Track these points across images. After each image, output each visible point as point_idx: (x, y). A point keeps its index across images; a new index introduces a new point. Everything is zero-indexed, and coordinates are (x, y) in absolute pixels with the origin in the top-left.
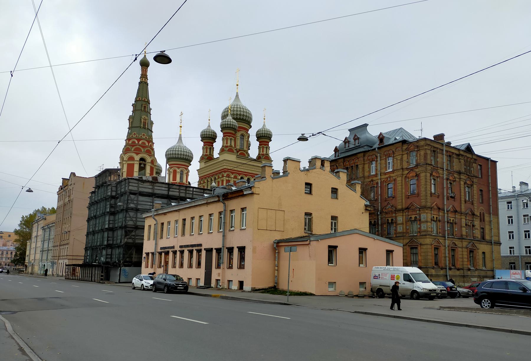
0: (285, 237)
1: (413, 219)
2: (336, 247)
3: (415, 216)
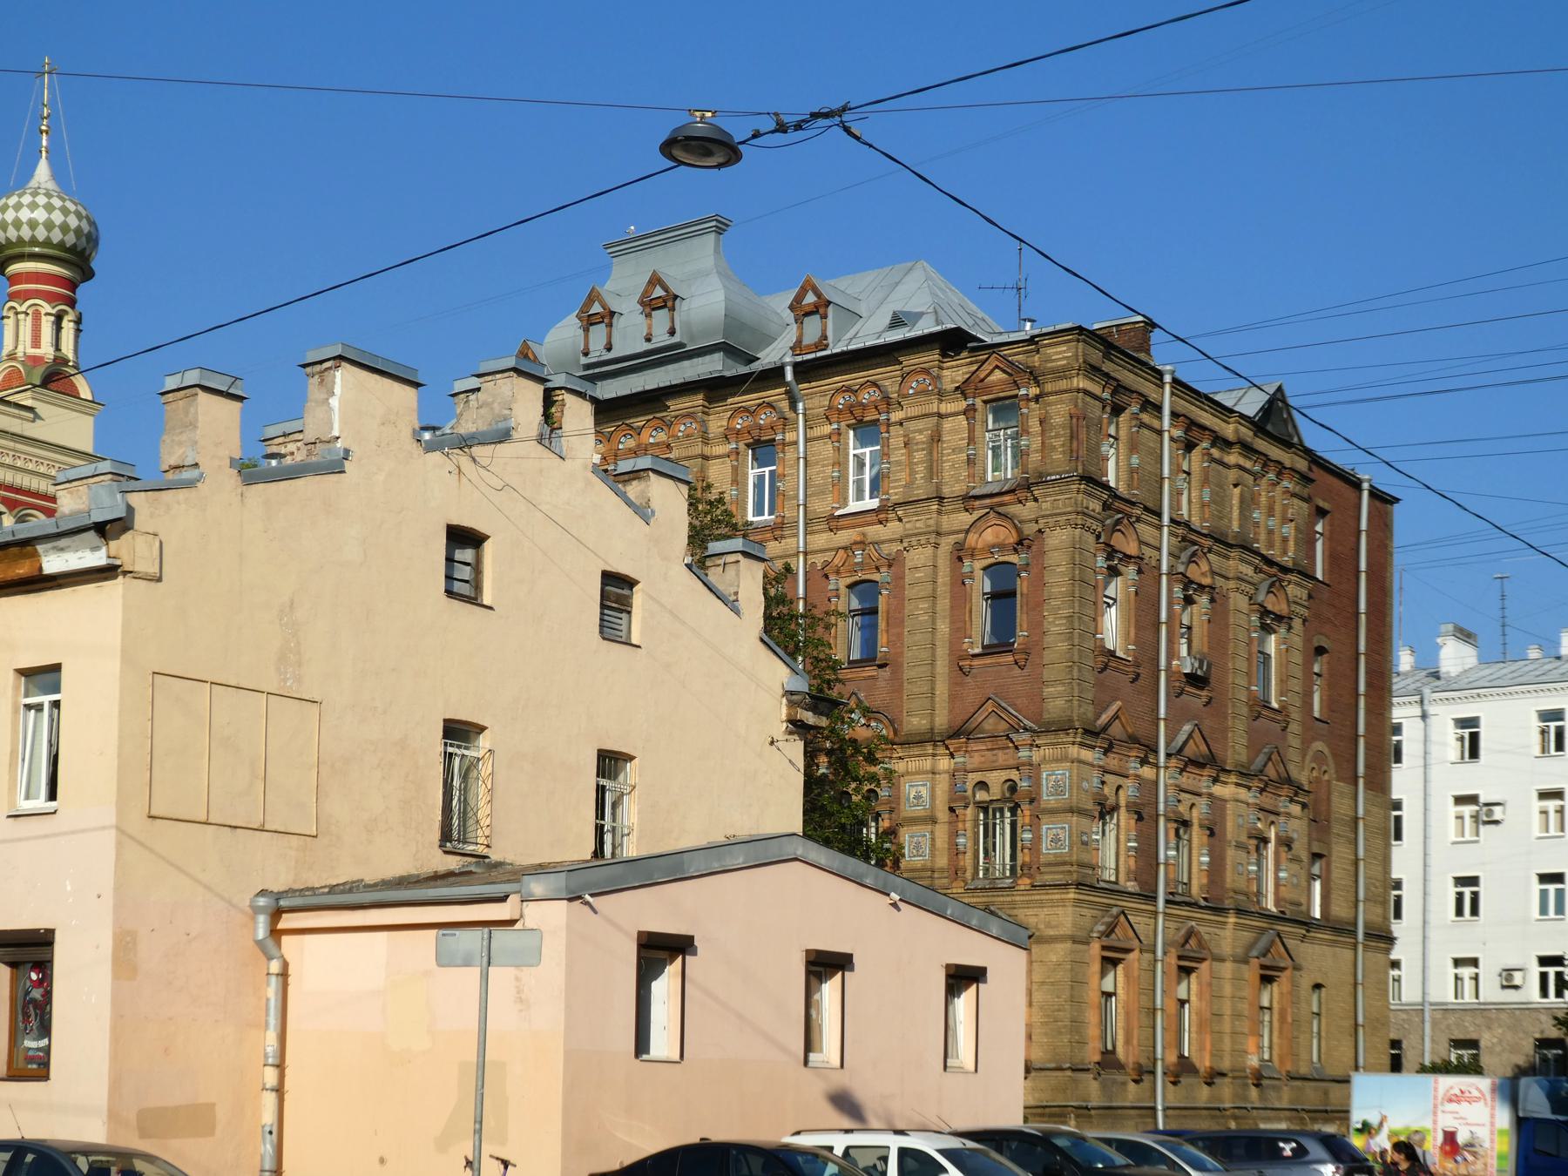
0: (320, 878)
1: (996, 791)
2: (679, 946)
3: (1004, 775)
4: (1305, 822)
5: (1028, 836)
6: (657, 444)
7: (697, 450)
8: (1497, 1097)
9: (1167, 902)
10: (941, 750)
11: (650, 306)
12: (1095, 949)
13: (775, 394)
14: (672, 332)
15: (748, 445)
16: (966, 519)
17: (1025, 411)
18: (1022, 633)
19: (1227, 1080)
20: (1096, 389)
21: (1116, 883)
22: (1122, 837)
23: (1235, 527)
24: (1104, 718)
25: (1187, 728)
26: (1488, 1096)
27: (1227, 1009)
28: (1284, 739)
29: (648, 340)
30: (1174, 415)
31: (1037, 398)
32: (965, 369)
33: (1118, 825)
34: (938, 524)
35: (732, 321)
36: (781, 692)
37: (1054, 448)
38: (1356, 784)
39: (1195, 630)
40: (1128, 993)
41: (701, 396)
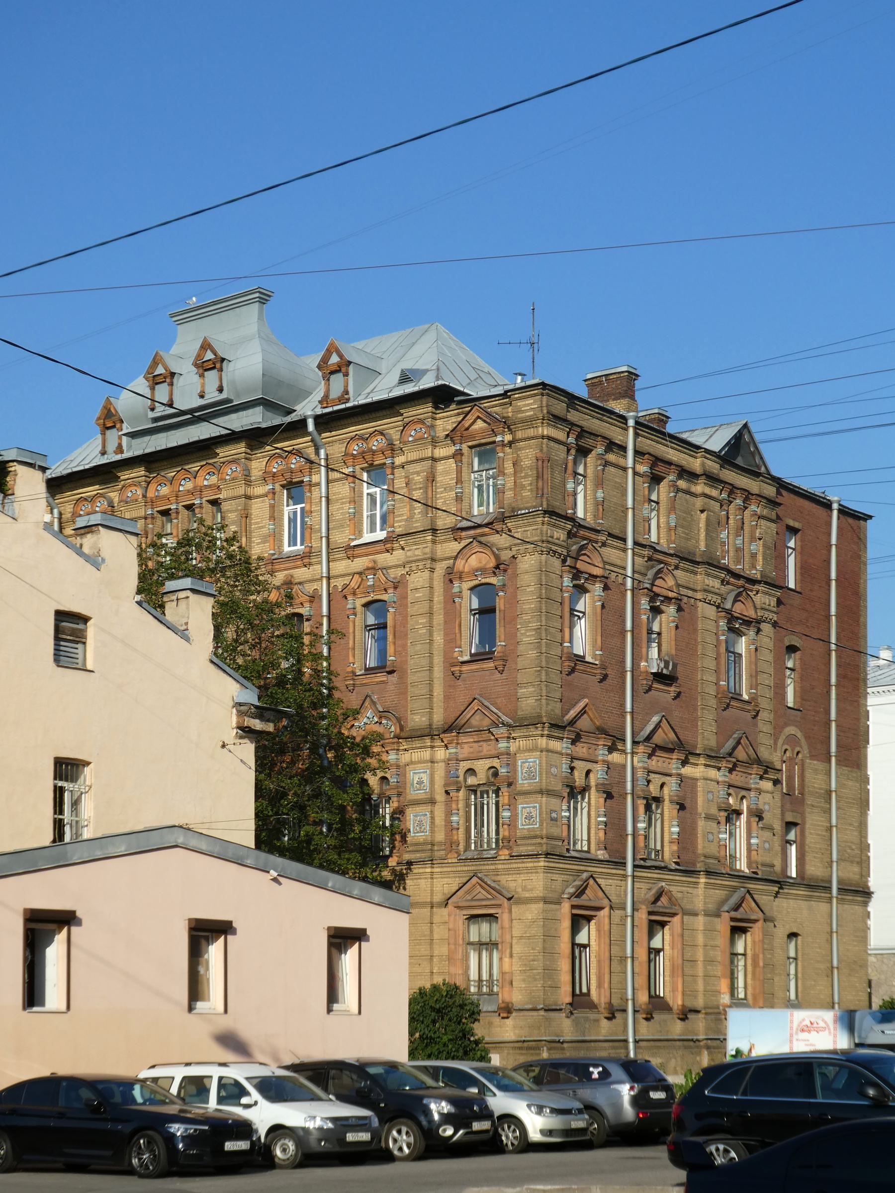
1: (481, 777)
2: (66, 919)
3: (488, 763)
4: (778, 796)
5: (506, 814)
6: (210, 486)
7: (241, 491)
8: (838, 1026)
9: (635, 866)
10: (438, 743)
11: (203, 367)
12: (565, 909)
13: (302, 443)
14: (221, 390)
15: (283, 486)
16: (456, 546)
17: (501, 455)
18: (500, 643)
19: (701, 1016)
20: (561, 435)
21: (588, 852)
22: (593, 814)
23: (702, 547)
24: (572, 713)
25: (655, 719)
26: (831, 1026)
27: (700, 955)
28: (756, 725)
29: (202, 397)
30: (637, 453)
31: (510, 443)
32: (454, 419)
33: (589, 803)
34: (433, 552)
35: (269, 378)
36: (231, 704)
37: (523, 487)
38: (829, 762)
39: (664, 635)
40: (599, 945)
41: (243, 444)
